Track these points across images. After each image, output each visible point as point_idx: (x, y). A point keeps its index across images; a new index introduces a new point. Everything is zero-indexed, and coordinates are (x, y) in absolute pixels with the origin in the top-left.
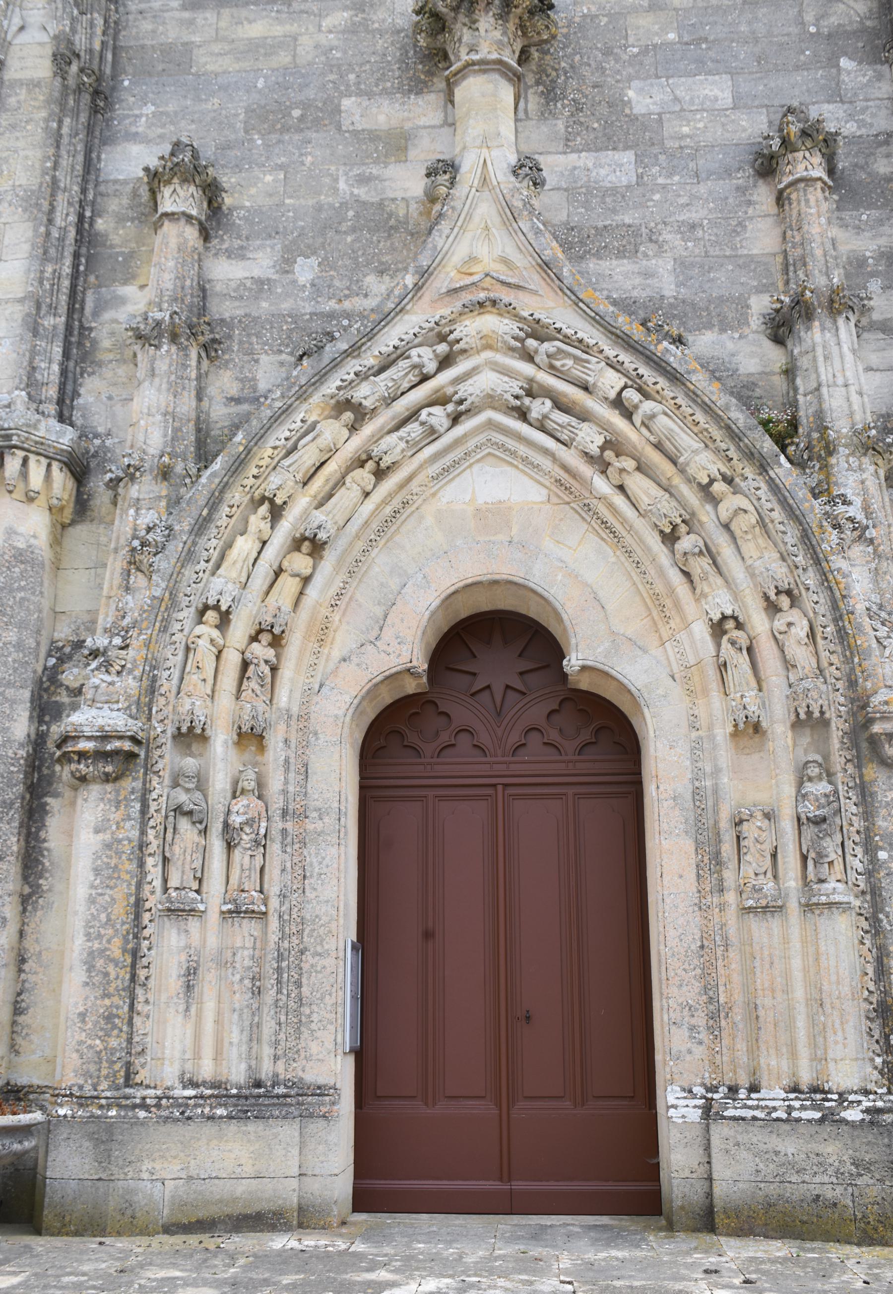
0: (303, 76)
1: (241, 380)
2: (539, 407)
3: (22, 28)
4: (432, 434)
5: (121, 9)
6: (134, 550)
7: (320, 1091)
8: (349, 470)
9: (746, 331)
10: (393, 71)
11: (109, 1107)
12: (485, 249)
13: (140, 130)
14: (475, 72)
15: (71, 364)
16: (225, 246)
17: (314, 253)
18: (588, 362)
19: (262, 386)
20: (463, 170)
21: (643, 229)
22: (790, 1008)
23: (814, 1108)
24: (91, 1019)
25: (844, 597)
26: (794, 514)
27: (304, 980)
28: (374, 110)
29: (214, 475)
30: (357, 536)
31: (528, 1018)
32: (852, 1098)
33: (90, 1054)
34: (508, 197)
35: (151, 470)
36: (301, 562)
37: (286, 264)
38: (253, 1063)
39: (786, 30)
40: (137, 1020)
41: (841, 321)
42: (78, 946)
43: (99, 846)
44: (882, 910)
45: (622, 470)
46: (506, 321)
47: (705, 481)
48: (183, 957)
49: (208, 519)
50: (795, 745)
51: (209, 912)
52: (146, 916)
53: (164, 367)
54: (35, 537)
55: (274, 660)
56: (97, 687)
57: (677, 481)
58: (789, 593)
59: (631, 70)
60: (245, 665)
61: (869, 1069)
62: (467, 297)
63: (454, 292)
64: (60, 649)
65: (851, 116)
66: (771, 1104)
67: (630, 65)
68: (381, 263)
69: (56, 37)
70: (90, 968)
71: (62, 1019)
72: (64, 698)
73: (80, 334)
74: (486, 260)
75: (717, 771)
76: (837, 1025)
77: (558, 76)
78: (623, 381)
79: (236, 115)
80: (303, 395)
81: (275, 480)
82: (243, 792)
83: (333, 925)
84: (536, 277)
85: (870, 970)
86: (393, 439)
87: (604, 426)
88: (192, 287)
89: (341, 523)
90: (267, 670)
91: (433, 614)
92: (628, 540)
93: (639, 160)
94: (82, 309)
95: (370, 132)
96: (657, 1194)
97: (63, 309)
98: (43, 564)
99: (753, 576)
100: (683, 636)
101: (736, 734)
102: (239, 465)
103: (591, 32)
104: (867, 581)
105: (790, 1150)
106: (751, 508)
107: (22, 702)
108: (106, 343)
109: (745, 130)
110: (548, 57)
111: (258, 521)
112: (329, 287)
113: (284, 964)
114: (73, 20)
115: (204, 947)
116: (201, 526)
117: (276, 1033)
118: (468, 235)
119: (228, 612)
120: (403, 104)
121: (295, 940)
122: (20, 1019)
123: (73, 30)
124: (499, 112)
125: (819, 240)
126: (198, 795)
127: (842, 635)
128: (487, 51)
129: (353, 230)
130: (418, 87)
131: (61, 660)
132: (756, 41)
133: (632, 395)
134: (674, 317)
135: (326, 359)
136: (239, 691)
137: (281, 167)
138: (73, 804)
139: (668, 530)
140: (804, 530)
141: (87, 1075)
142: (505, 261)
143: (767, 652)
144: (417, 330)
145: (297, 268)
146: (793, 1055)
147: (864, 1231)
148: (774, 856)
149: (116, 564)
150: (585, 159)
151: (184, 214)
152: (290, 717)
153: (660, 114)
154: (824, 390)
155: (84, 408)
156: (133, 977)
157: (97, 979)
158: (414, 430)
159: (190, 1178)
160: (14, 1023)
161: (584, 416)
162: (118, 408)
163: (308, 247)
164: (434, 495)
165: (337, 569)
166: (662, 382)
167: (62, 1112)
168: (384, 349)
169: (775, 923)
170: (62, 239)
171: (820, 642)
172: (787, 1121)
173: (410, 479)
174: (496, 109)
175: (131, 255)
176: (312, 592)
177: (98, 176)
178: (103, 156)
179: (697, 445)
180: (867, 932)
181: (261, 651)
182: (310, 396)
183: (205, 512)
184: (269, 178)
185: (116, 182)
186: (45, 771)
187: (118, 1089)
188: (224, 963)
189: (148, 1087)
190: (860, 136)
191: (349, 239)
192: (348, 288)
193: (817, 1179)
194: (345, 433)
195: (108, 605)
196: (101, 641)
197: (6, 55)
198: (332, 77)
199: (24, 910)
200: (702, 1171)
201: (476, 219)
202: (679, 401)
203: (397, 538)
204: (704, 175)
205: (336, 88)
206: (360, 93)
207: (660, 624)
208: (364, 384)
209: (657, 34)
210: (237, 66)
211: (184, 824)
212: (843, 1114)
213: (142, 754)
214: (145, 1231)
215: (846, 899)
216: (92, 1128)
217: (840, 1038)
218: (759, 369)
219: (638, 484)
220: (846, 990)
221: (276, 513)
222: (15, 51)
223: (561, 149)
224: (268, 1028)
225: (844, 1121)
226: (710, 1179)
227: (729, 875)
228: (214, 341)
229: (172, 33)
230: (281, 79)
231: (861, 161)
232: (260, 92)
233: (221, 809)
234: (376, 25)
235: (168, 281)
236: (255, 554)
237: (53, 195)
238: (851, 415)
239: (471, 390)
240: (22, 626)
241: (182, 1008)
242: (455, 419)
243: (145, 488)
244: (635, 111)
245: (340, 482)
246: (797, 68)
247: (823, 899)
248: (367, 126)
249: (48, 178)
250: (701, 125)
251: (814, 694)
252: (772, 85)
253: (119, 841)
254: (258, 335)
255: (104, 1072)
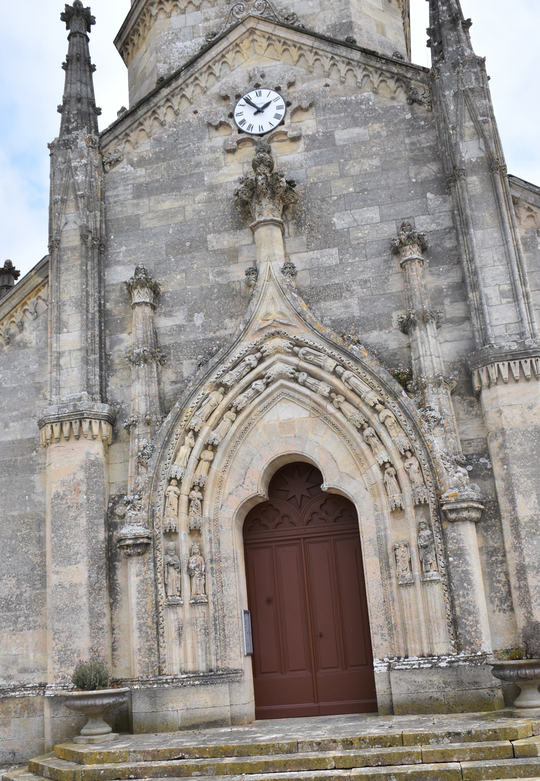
0: (189, 226)
1: (176, 373)
2: (302, 377)
3: (66, 223)
4: (258, 393)
5: (107, 202)
6: (139, 456)
7: (236, 671)
8: (224, 412)
9: (391, 329)
10: (228, 219)
11: (154, 684)
12: (273, 308)
13: (121, 259)
14: (262, 225)
15: (103, 373)
16: (163, 311)
17: (202, 311)
18: (320, 356)
19: (186, 375)
20: (261, 273)
21: (344, 285)
22: (419, 624)
23: (429, 663)
24: (143, 651)
25: (431, 451)
26: (409, 417)
27: (226, 628)
28: (222, 239)
29: (168, 422)
30: (231, 441)
31: (321, 635)
32: (442, 658)
33: (144, 664)
34: (281, 284)
35: (142, 421)
36: (208, 455)
37: (190, 317)
38: (208, 663)
39: (402, 182)
40: (161, 650)
41: (428, 326)
42: (135, 622)
43: (139, 582)
44: (451, 582)
45: (339, 402)
46: (284, 341)
47: (373, 405)
48: (176, 623)
49: (168, 441)
50: (416, 515)
51: (185, 604)
52: (160, 608)
53: (143, 374)
54: (98, 454)
55: (201, 497)
56: (131, 517)
57: (361, 405)
58: (410, 450)
59: (334, 208)
60: (190, 501)
61: (450, 646)
62: (267, 332)
63: (261, 330)
64: (113, 499)
65: (433, 221)
66: (412, 662)
67: (334, 205)
68: (231, 313)
69: (81, 227)
70: (141, 631)
71: (132, 651)
72: (118, 520)
73: (105, 358)
74: (274, 313)
75: (385, 529)
76: (436, 629)
77: (302, 214)
78: (336, 362)
79: (162, 248)
80: (202, 383)
81: (194, 421)
82: (194, 554)
83: (236, 605)
84: (295, 319)
85: (448, 606)
86: (241, 397)
87: (330, 383)
88: (151, 335)
89: (223, 436)
90: (199, 502)
91: (265, 471)
92: (344, 431)
93: (340, 252)
94: (105, 346)
95: (221, 250)
96: (376, 703)
97: (97, 351)
98: (102, 465)
99: (395, 444)
100: (368, 471)
101: (392, 512)
102: (178, 417)
103: (315, 191)
104: (441, 443)
105: (420, 680)
106: (392, 415)
107: (101, 524)
108: (117, 361)
109: (386, 232)
110: (297, 205)
111: (189, 439)
112: (209, 326)
113: (217, 622)
114: (87, 217)
115: (184, 618)
116: (165, 445)
117: (216, 650)
118: (265, 302)
119: (180, 480)
120: (234, 235)
121: (221, 612)
122: (115, 653)
123: (88, 221)
124: (274, 244)
125: (417, 287)
126: (176, 557)
127: (431, 468)
128: (267, 216)
129: (217, 298)
130: (239, 226)
131: (115, 504)
132: (389, 188)
133: (340, 369)
134: (360, 325)
135: (210, 367)
136: (188, 512)
137: (184, 271)
138: (126, 564)
139: (359, 427)
140: (414, 424)
141: (144, 672)
142: (281, 313)
143: (403, 476)
144: (247, 349)
145: (195, 318)
146: (421, 642)
147: (449, 709)
148: (410, 562)
149: (132, 463)
150: (316, 254)
151: (144, 302)
152: (210, 521)
153: (348, 228)
154: (421, 359)
155: (111, 392)
156: (158, 633)
157: (144, 635)
158: (250, 392)
159: (188, 709)
160: (113, 655)
161: (321, 379)
162: (125, 390)
163: (199, 308)
164: (262, 418)
165: (224, 456)
166: (352, 363)
167: (136, 687)
168: (234, 359)
169: (411, 590)
170: (93, 318)
171: (423, 471)
172: (418, 669)
173: (250, 413)
174: (272, 242)
175: (123, 319)
176: (214, 467)
177: (105, 283)
178: (106, 273)
179: (368, 389)
180: (446, 591)
181: (196, 494)
182: (205, 383)
183: (166, 439)
184: (179, 277)
185: (113, 285)
186: (113, 551)
187: (156, 677)
188: (193, 624)
189: (168, 675)
190: (438, 230)
191: (216, 303)
192: (218, 326)
193: (430, 691)
194: (222, 396)
195: (131, 480)
196: (130, 497)
197: (60, 236)
198: (202, 225)
199: (112, 609)
200: (388, 692)
201: (268, 294)
202: (359, 371)
203: (248, 439)
204: (369, 256)
205: (204, 230)
206: (215, 232)
207: (360, 467)
208: (227, 375)
209: (344, 189)
210: (160, 224)
211: (171, 570)
212: (439, 664)
213: (152, 543)
214: (172, 730)
215: (438, 578)
216: (148, 692)
217: (437, 634)
218: (398, 346)
219: (346, 407)
220: (439, 615)
221: (196, 435)
222: (64, 234)
223: (305, 250)
224: (213, 648)
225: (440, 667)
226: (391, 694)
227: (392, 571)
228: (163, 356)
229: (130, 211)
230: (179, 228)
231: (439, 242)
232: (171, 235)
233: (185, 562)
234: (219, 198)
235: (140, 334)
236: (189, 453)
237: (87, 299)
238: (433, 369)
239: (272, 372)
240: (97, 493)
241: (178, 643)
242: (267, 385)
243: (141, 429)
244: (337, 228)
245: (221, 418)
246: (408, 200)
247: (428, 579)
248: (219, 247)
249: (84, 293)
250: (366, 232)
251: (422, 494)
252: (397, 209)
253: (147, 579)
254: (181, 352)
255: (150, 671)
